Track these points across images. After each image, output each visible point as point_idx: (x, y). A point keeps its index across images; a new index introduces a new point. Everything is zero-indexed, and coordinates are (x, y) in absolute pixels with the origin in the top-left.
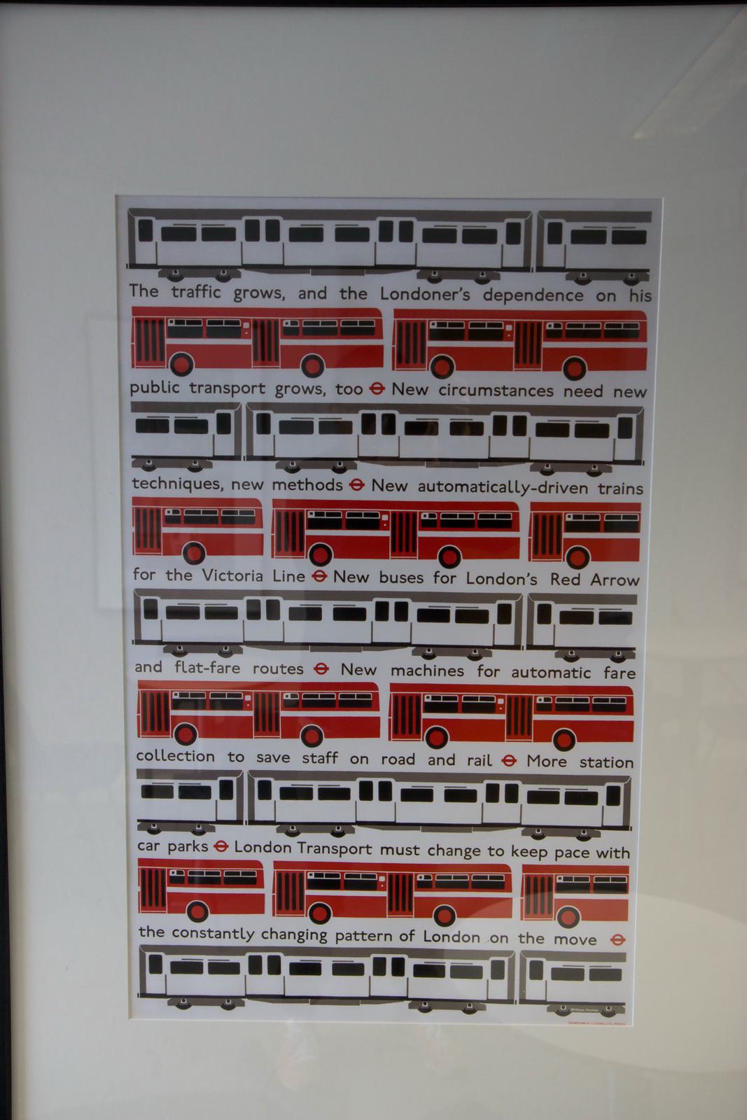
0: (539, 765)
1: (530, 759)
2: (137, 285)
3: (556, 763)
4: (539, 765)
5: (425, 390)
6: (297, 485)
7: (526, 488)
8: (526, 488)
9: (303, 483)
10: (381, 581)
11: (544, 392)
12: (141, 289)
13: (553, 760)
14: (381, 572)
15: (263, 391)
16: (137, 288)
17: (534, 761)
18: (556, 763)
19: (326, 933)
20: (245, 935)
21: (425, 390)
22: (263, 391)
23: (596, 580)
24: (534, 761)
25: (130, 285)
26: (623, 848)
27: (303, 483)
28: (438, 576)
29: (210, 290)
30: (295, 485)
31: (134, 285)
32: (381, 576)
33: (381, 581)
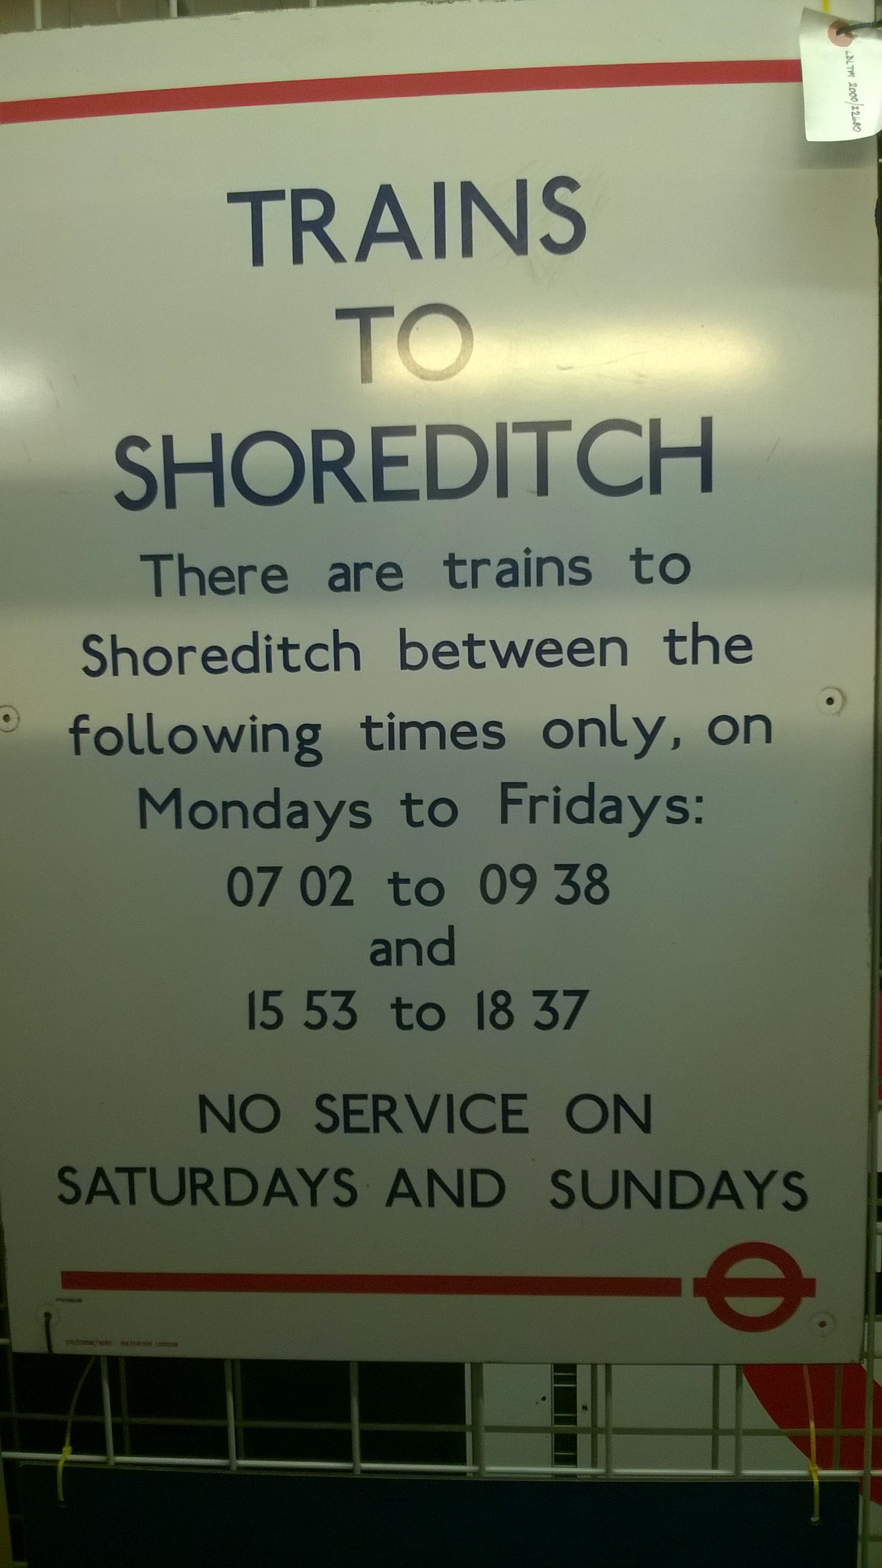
0: (178, 825)
1: (148, 804)
2: (169, 557)
3: (193, 660)
4: (178, 825)
5: (233, 737)
6: (464, 651)
7: (649, 730)
8: (649, 730)
9: (684, 639)
10: (404, 665)
11: (473, 733)
12: (183, 571)
13: (182, 651)
14: (403, 631)
15: (478, 660)
16: (169, 569)
17: (160, 809)
18: (193, 660)
19: (315, 728)
20: (627, 728)
21: (233, 737)
22: (478, 660)
23: (387, 224)
24: (160, 809)
25: (144, 558)
26: (695, 625)
27: (684, 639)
28: (86, 730)
29: (557, 799)
30: (455, 652)
31: (156, 559)
32: (404, 646)
33: (404, 665)
